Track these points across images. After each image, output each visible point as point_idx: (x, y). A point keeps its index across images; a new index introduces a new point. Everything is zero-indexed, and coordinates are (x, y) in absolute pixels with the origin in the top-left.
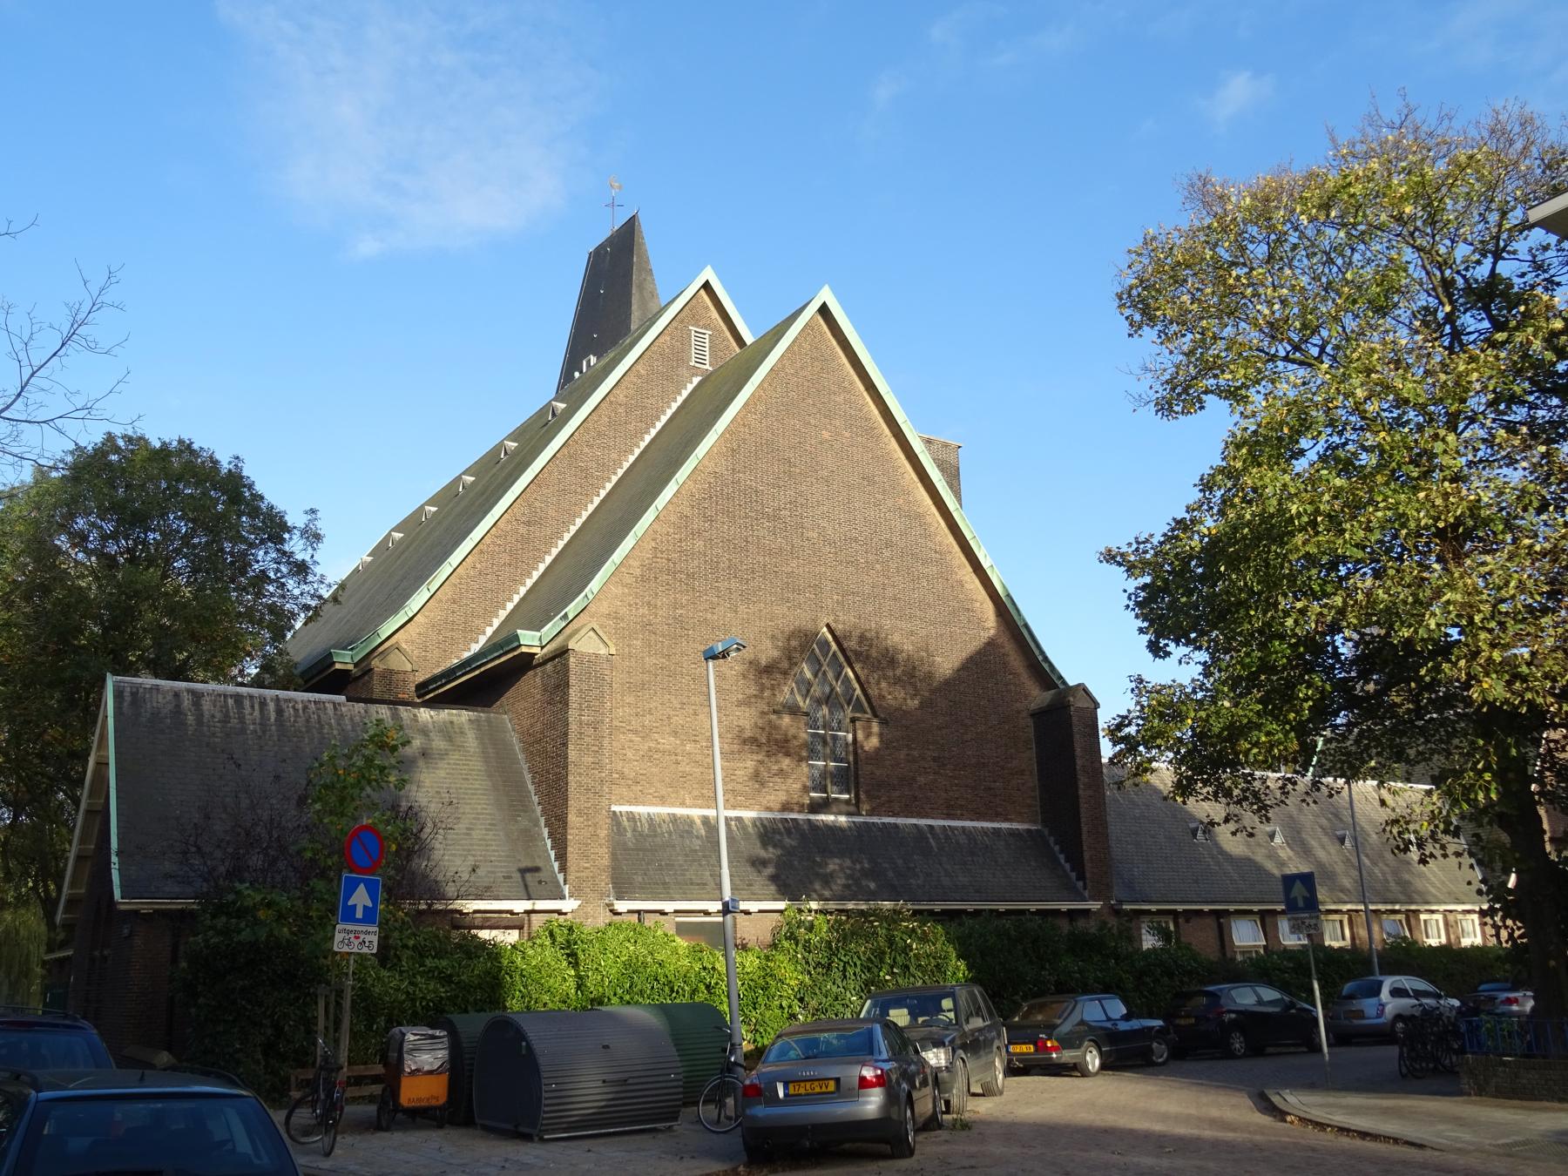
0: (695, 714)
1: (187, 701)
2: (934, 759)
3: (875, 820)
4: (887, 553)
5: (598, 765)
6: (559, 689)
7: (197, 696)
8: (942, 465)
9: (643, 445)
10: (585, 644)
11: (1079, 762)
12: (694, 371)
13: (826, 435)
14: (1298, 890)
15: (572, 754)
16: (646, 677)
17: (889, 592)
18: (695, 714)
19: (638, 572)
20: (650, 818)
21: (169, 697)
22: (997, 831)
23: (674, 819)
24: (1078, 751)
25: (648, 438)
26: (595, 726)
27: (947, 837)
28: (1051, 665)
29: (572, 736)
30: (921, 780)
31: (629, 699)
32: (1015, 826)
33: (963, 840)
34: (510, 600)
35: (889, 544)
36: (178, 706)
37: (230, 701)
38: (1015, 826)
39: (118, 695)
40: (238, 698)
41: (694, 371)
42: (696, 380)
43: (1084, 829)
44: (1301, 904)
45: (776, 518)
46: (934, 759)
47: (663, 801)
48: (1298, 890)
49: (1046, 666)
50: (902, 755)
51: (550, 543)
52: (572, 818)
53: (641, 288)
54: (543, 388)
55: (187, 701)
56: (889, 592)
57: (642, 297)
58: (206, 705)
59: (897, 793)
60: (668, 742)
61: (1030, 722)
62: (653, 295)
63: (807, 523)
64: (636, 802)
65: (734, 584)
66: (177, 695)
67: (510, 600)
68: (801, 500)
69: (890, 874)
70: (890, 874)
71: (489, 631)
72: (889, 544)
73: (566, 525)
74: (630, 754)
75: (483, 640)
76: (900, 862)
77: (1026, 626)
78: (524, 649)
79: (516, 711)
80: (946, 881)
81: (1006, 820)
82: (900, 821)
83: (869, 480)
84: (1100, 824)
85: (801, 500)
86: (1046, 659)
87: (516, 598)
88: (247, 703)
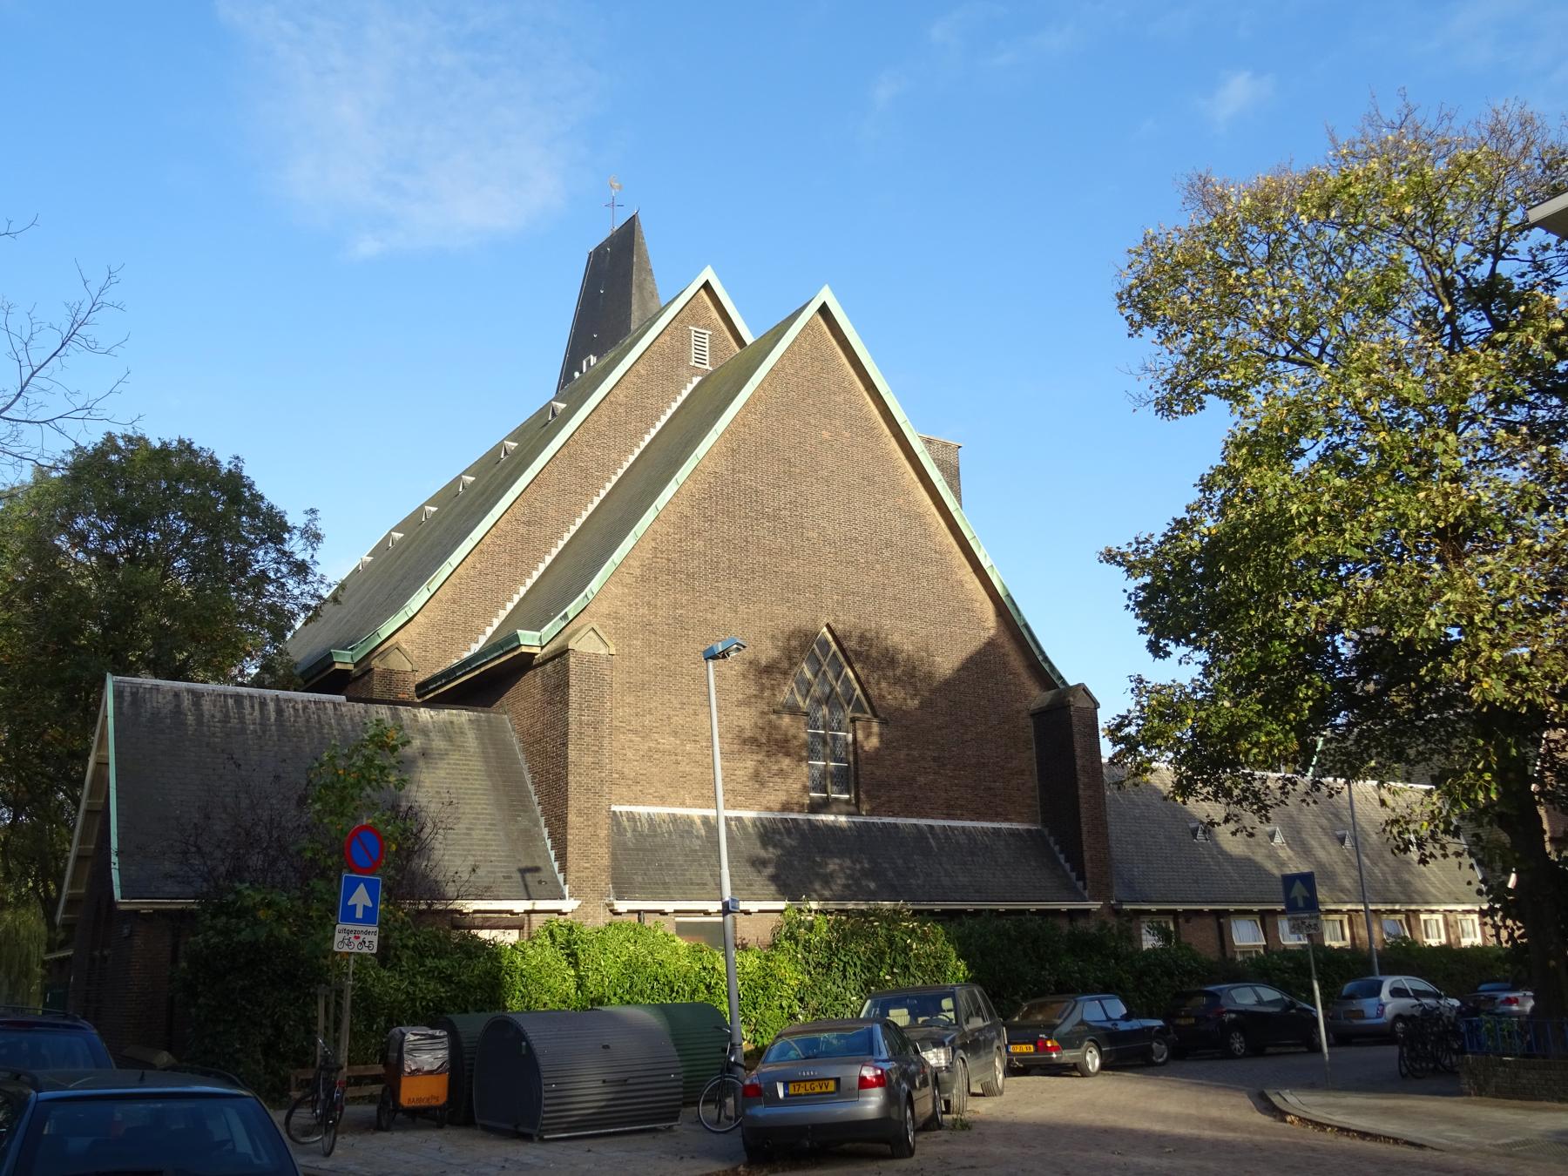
0: (695, 714)
1: (187, 701)
2: (934, 759)
3: (875, 820)
4: (887, 553)
5: (598, 765)
6: (559, 689)
7: (197, 696)
8: (942, 465)
9: (643, 445)
10: (585, 644)
11: (1079, 762)
12: (694, 371)
13: (826, 435)
14: (1298, 890)
15: (572, 754)
16: (646, 677)
17: (889, 592)
18: (695, 714)
19: (638, 572)
20: (650, 818)
21: (169, 697)
22: (997, 831)
23: (674, 819)
24: (1078, 751)
25: (648, 438)
26: (595, 726)
27: (947, 837)
28: (1051, 665)
29: (572, 736)
30: (921, 780)
31: (629, 699)
32: (1015, 826)
33: (963, 840)
34: (510, 600)
35: (889, 544)
36: (178, 706)
37: (230, 701)
38: (1015, 826)
39: (118, 695)
40: (238, 698)
41: (694, 371)
42: (696, 380)
43: (1084, 829)
44: (1301, 904)
45: (776, 518)
46: (934, 759)
47: (663, 801)
48: (1298, 890)
49: (1046, 666)
50: (902, 755)
51: (550, 543)
52: (572, 818)
53: (641, 288)
54: (543, 388)
55: (187, 701)
56: (889, 592)
57: (642, 297)
58: (206, 705)
59: (897, 793)
60: (668, 742)
61: (1030, 722)
62: (653, 295)
63: (807, 523)
64: (636, 802)
65: (734, 584)
66: (177, 695)
67: (510, 600)
68: (801, 500)
69: (890, 874)
70: (890, 874)
71: (489, 631)
72: (889, 544)
73: (566, 525)
74: (630, 754)
75: (483, 640)
76: (900, 862)
77: (1026, 626)
78: (524, 649)
79: (516, 711)
80: (946, 881)
81: (1006, 820)
82: (900, 821)
83: (869, 480)
84: (1100, 824)
85: (801, 500)
86: (1046, 659)
87: (516, 598)
88: (247, 703)
